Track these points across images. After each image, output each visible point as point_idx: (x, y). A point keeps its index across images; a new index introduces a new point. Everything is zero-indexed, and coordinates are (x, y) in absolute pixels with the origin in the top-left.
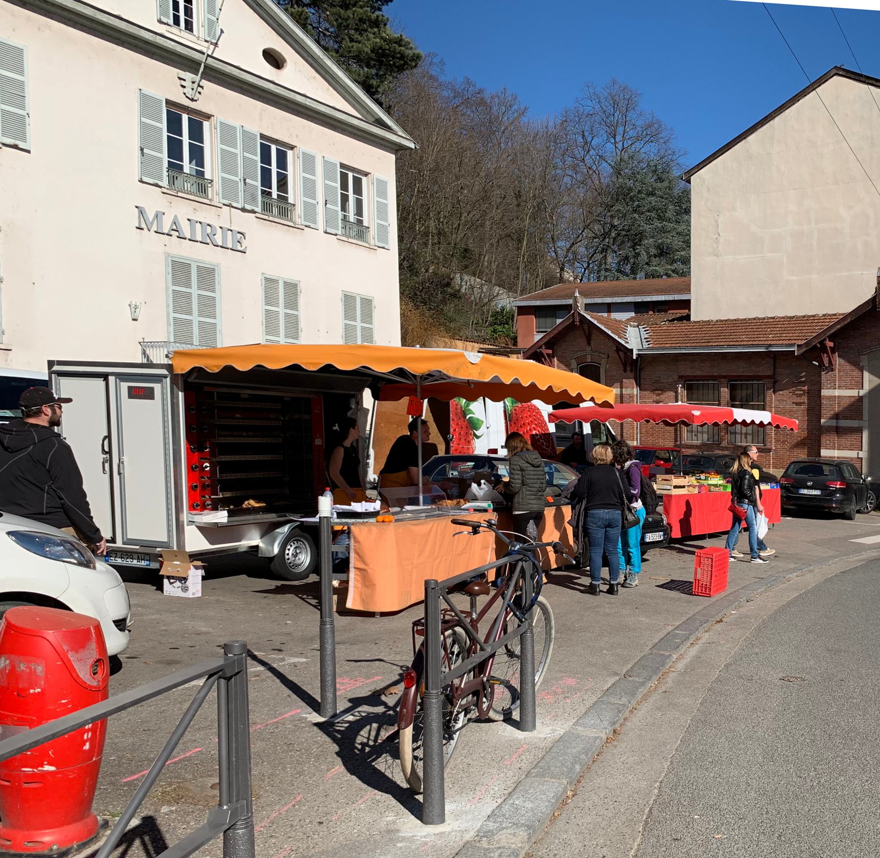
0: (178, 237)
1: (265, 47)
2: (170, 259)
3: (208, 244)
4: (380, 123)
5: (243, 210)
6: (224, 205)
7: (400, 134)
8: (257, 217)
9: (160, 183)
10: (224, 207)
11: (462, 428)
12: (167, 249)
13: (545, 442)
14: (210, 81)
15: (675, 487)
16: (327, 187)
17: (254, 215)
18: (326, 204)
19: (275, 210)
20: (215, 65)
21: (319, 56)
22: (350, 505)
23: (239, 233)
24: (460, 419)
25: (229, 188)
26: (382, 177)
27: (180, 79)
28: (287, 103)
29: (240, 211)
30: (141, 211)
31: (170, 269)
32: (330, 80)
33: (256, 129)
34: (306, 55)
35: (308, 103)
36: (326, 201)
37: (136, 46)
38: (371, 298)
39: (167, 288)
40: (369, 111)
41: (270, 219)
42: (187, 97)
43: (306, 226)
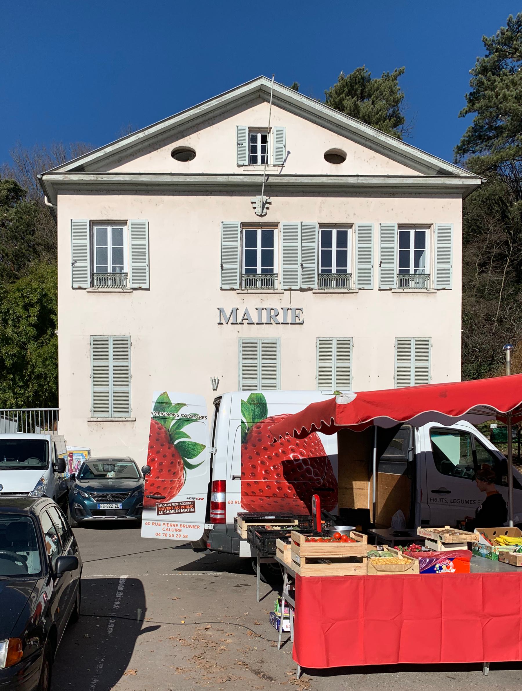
0: (248, 324)
1: (325, 152)
2: (241, 341)
3: (272, 324)
4: (443, 173)
5: (302, 290)
6: (285, 290)
7: (464, 175)
8: (313, 293)
9: (235, 287)
10: (285, 292)
11: (165, 456)
12: (240, 335)
13: (314, 467)
14: (277, 196)
15: (310, 561)
16: (383, 250)
17: (311, 292)
18: (380, 264)
19: (334, 283)
20: (275, 181)
21: (373, 136)
22: (444, 527)
23: (297, 309)
24: (162, 445)
25: (289, 275)
26: (444, 223)
27: (252, 203)
28: (343, 189)
29: (299, 292)
30: (221, 310)
31: (241, 349)
32: (389, 153)
33: (314, 221)
34: (364, 141)
35: (359, 181)
36: (381, 262)
37: (220, 191)
38: (427, 339)
39: (239, 363)
40: (429, 166)
41: (325, 292)
42: (258, 215)
43: (359, 289)
